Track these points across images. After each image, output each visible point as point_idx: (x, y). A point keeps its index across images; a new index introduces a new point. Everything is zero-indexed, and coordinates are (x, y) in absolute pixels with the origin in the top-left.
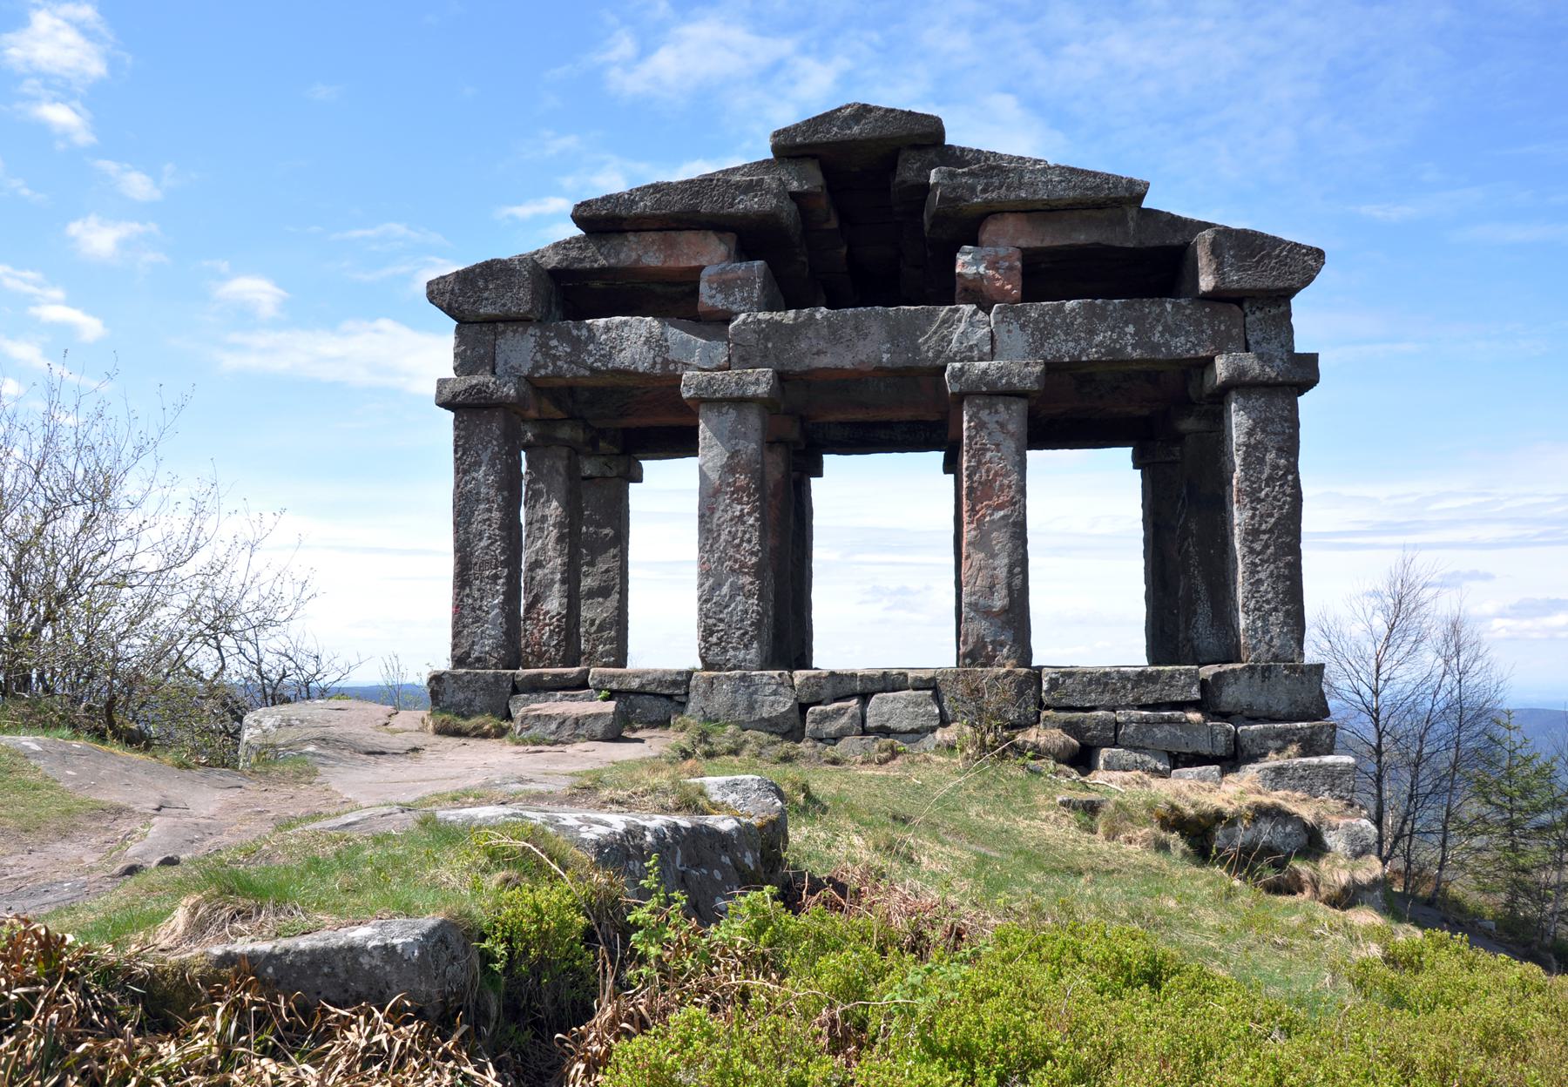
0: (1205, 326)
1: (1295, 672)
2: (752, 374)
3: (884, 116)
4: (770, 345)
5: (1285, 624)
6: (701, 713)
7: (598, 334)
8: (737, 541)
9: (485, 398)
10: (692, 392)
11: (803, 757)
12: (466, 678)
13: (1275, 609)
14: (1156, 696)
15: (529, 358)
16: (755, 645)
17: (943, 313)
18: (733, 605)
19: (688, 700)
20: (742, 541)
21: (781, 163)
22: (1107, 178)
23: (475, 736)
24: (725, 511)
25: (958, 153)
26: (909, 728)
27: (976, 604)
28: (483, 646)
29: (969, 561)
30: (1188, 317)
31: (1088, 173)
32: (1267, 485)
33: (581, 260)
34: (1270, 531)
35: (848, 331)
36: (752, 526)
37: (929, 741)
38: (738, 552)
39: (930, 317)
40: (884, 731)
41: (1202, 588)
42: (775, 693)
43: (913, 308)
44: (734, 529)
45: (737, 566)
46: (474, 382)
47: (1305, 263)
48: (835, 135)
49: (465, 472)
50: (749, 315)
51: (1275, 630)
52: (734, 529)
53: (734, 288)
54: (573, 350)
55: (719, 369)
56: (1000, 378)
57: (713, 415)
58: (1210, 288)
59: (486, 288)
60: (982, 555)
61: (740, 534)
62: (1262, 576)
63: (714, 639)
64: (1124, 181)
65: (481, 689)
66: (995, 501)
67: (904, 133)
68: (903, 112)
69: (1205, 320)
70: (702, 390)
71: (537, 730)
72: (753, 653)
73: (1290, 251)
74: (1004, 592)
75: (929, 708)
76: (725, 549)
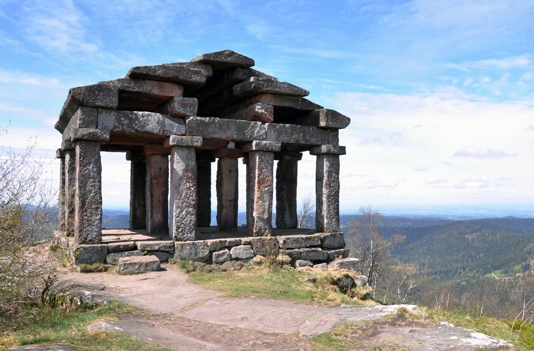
0: (319, 136)
1: (340, 235)
2: (196, 138)
3: (238, 56)
4: (200, 129)
5: (336, 221)
6: (179, 257)
7: (139, 117)
8: (188, 196)
9: (96, 138)
10: (175, 143)
11: (214, 270)
12: (90, 249)
13: (334, 217)
14: (310, 244)
15: (112, 124)
16: (194, 232)
17: (252, 124)
18: (186, 218)
19: (174, 253)
20: (190, 196)
21: (200, 64)
22: (299, 88)
23: (96, 272)
24: (184, 185)
25: (254, 71)
26: (245, 258)
27: (260, 217)
28: (92, 235)
29: (258, 203)
30: (315, 132)
31: (295, 86)
32: (333, 183)
33: (129, 88)
34: (333, 196)
35: (225, 126)
36: (193, 191)
37: (251, 262)
38: (188, 200)
39: (249, 124)
40: (237, 259)
41: (287, 206)
42: (203, 248)
43: (244, 121)
44: (187, 192)
45: (188, 205)
46: (92, 131)
47: (345, 122)
48: (223, 60)
49: (84, 166)
50: (194, 117)
51: (334, 223)
52: (187, 192)
53: (187, 107)
54: (130, 122)
55: (182, 135)
56: (270, 147)
57: (180, 151)
58: (325, 126)
59: (99, 95)
60: (261, 202)
61: (189, 194)
62: (331, 208)
63: (180, 230)
64: (304, 90)
65: (95, 253)
66: (266, 185)
67: (244, 63)
68: (244, 56)
69: (319, 134)
70: (179, 142)
71: (131, 269)
72: (193, 235)
73: (343, 118)
74: (267, 213)
75: (250, 251)
76: (184, 198)
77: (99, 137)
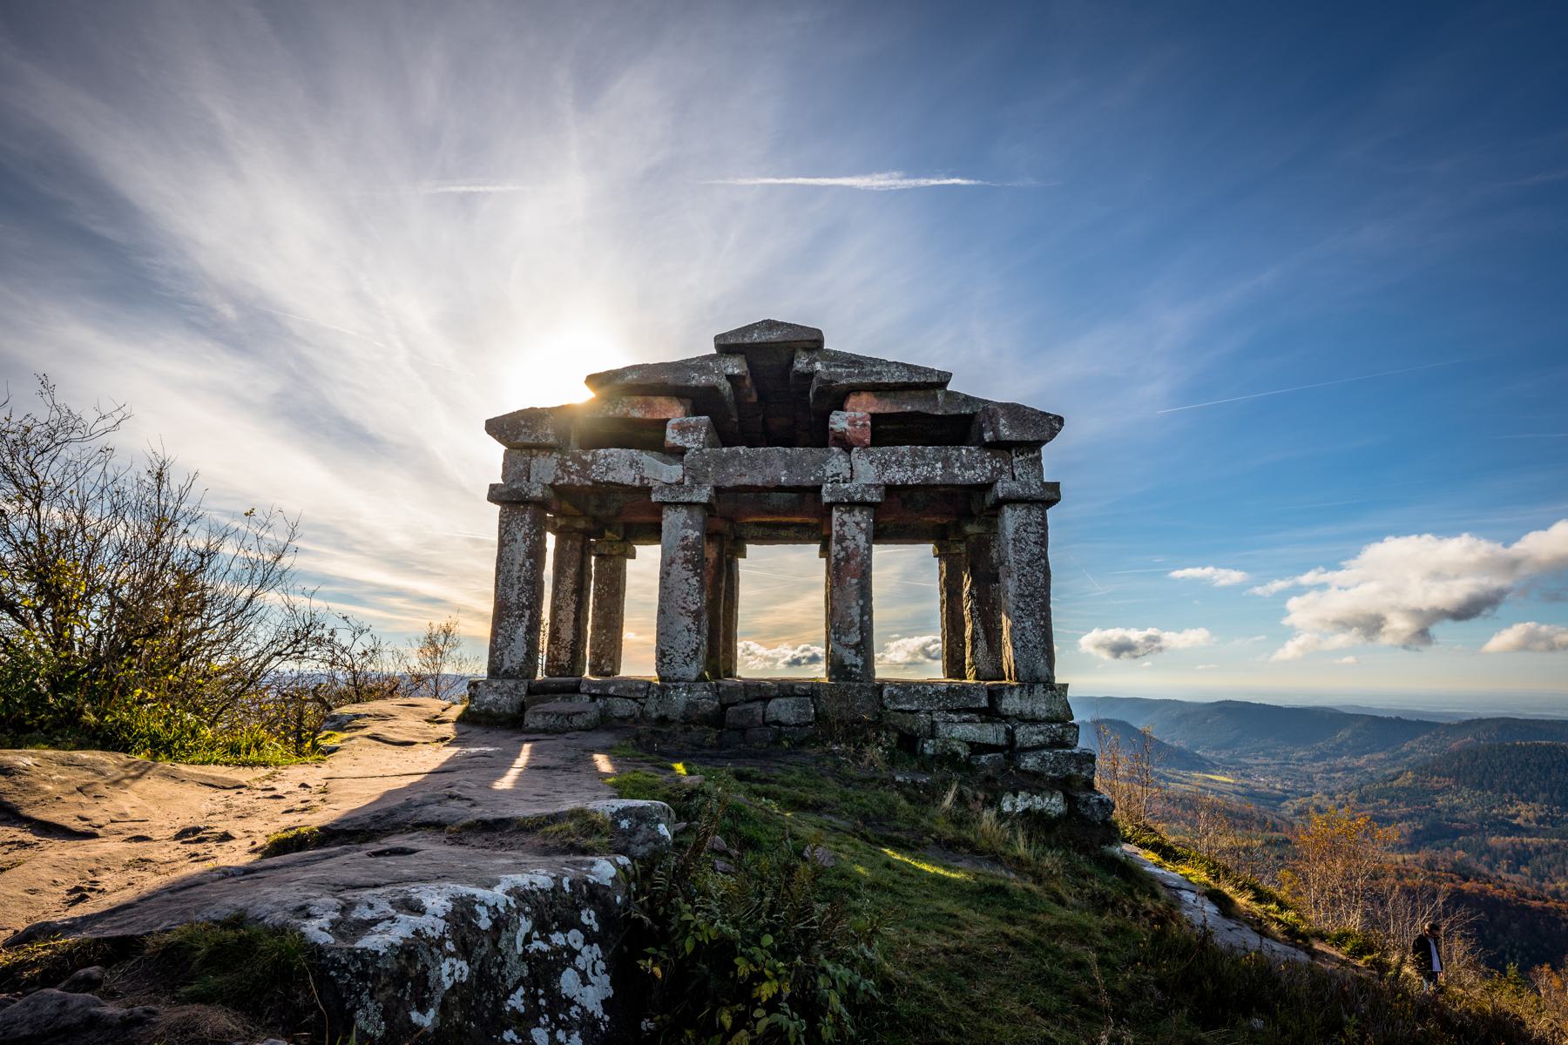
35: (760, 462)
47: (1050, 424)
77: (526, 494)
